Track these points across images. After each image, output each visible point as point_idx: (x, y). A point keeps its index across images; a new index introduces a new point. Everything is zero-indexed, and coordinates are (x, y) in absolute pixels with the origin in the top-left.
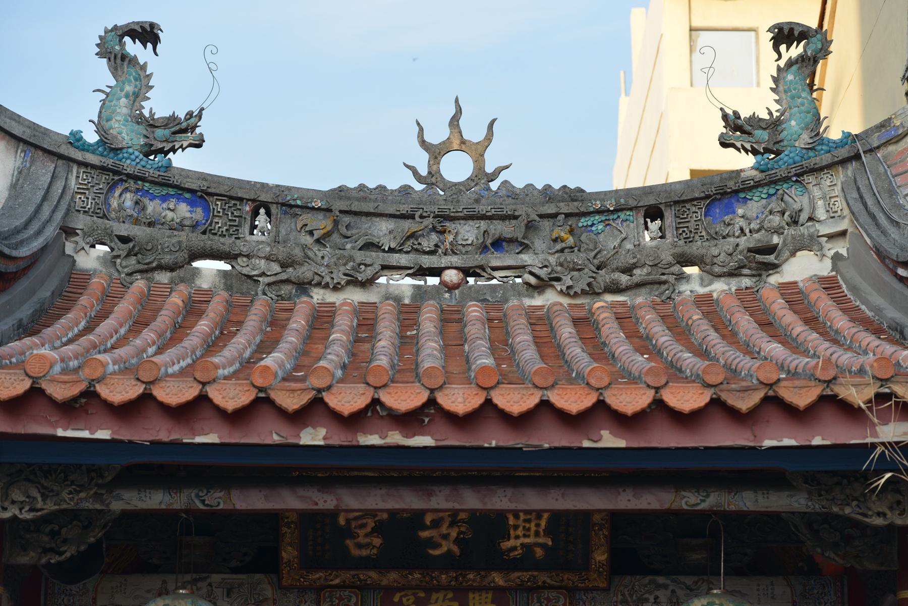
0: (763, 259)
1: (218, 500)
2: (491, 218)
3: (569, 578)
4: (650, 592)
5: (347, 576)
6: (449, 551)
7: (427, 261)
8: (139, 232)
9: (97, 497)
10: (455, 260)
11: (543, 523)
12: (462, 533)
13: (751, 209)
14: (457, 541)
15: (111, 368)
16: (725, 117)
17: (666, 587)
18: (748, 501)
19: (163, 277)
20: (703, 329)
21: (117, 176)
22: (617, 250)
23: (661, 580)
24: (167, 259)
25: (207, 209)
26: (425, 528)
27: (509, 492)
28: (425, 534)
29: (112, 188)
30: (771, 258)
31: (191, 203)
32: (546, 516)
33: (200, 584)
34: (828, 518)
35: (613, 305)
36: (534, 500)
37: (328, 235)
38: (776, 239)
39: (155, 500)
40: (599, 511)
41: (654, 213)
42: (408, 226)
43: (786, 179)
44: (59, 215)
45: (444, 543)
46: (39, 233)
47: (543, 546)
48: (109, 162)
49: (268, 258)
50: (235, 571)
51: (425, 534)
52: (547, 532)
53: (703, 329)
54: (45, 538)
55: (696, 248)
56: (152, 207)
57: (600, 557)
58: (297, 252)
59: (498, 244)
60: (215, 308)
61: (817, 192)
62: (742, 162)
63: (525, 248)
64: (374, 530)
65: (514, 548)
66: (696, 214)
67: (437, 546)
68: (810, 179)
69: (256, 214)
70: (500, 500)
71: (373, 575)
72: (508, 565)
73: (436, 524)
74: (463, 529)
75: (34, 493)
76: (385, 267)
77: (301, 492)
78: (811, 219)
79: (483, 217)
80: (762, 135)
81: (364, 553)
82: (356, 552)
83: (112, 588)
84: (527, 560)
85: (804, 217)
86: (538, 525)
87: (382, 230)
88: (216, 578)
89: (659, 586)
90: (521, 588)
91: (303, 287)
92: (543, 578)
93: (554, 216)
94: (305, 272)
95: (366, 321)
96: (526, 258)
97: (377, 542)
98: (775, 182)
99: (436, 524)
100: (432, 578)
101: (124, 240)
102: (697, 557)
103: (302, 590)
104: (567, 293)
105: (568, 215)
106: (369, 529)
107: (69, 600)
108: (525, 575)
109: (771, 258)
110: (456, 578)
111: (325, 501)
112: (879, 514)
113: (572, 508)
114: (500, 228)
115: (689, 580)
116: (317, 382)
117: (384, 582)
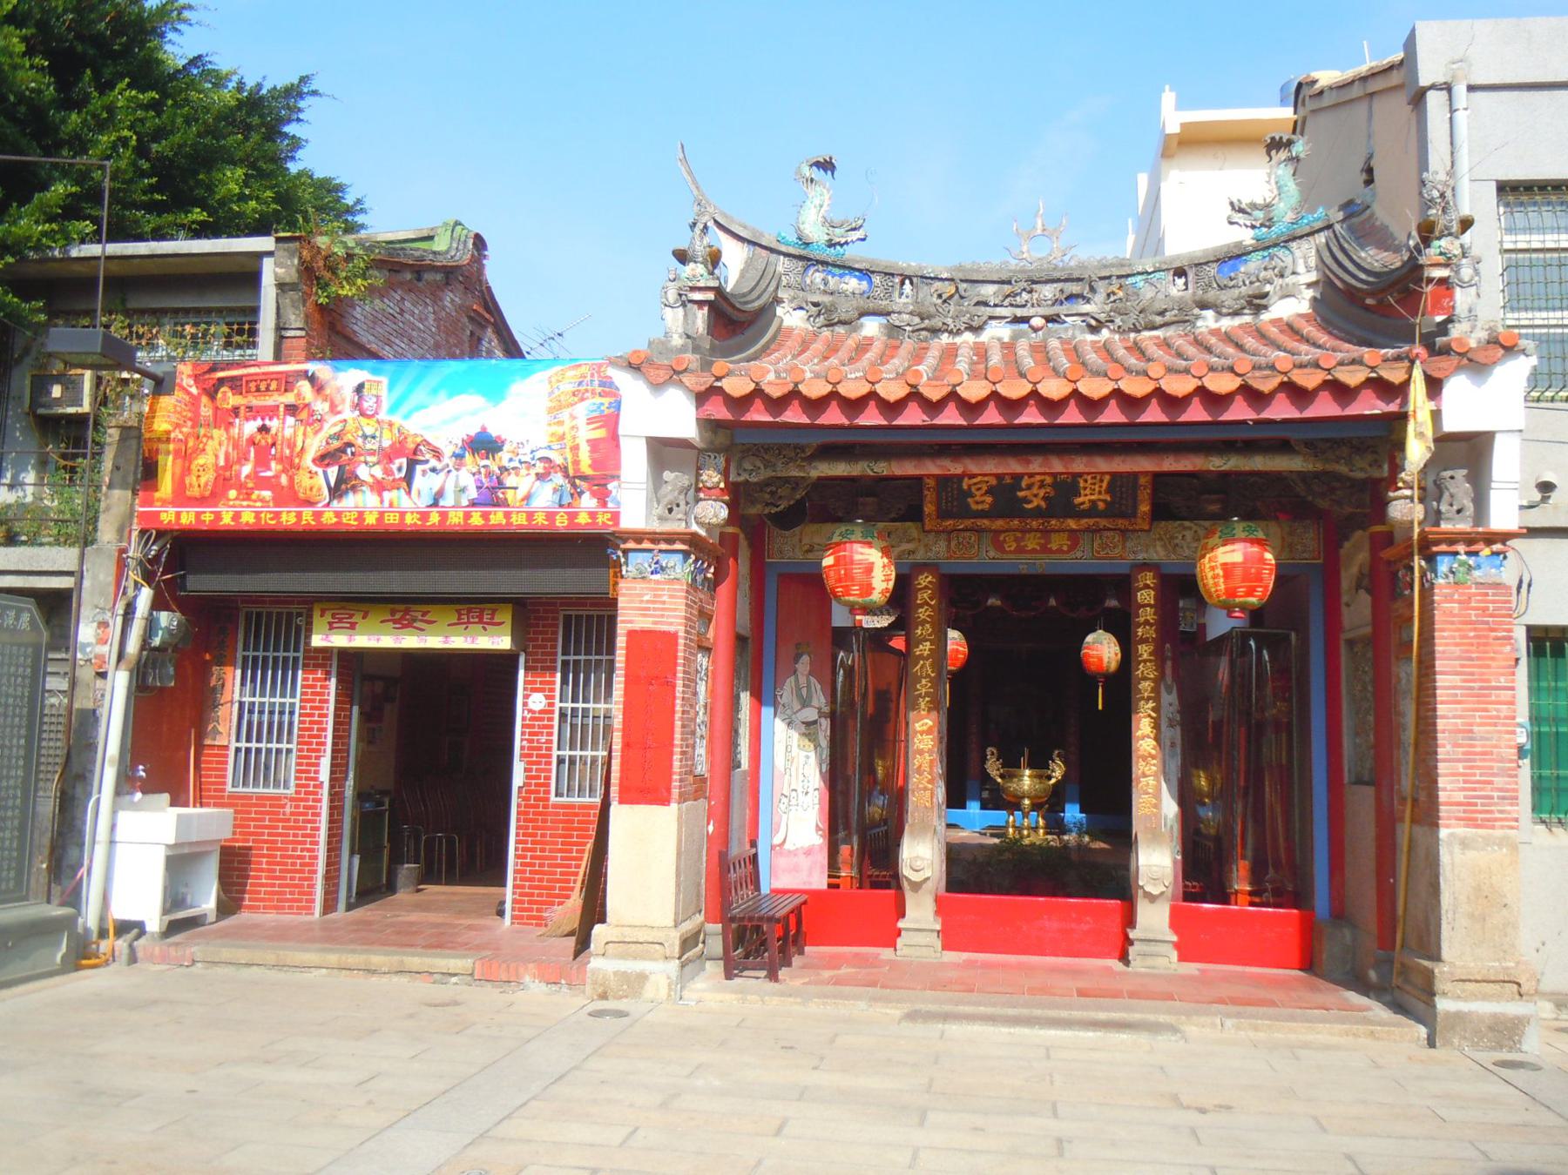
0: (1257, 303)
1: (882, 468)
2: (1066, 280)
3: (1121, 523)
5: (968, 523)
7: (1019, 312)
8: (826, 299)
9: (801, 468)
10: (1042, 311)
11: (1104, 485)
13: (1254, 264)
14: (1044, 498)
15: (808, 375)
16: (1232, 204)
18: (1259, 463)
19: (840, 330)
20: (1219, 346)
21: (808, 261)
22: (1153, 299)
23: (1187, 523)
24: (844, 317)
25: (870, 282)
27: (1085, 459)
28: (1021, 494)
29: (806, 269)
30: (1263, 302)
31: (860, 279)
34: (1325, 473)
35: (1151, 338)
36: (1103, 465)
37: (951, 297)
38: (1268, 288)
39: (840, 469)
40: (1146, 473)
41: (1180, 272)
42: (1007, 289)
43: (1275, 245)
44: (771, 289)
46: (759, 297)
48: (803, 253)
49: (911, 313)
50: (893, 520)
51: (1021, 494)
52: (1108, 491)
53: (1219, 346)
54: (767, 496)
55: (1212, 295)
56: (832, 281)
57: (1145, 508)
58: (932, 310)
59: (1071, 297)
60: (877, 348)
61: (1298, 253)
62: (1246, 237)
63: (1088, 301)
66: (1212, 270)
67: (1030, 502)
68: (1294, 245)
69: (902, 283)
70: (1079, 465)
72: (1080, 514)
73: (1029, 487)
75: (759, 464)
76: (991, 318)
77: (939, 462)
78: (1294, 273)
79: (1058, 280)
80: (1260, 214)
81: (980, 507)
82: (974, 507)
84: (1093, 511)
85: (1288, 272)
87: (989, 291)
88: (881, 525)
89: (1185, 528)
90: (1088, 530)
91: (935, 332)
92: (1103, 522)
93: (1109, 277)
94: (937, 322)
95: (982, 352)
96: (1086, 308)
97: (989, 499)
98: (1268, 248)
99: (1029, 487)
101: (815, 305)
102: (1214, 508)
103: (938, 532)
104: (1119, 330)
105: (1119, 277)
108: (1091, 521)
109: (1263, 302)
111: (955, 468)
112: (1362, 469)
114: (1074, 288)
115: (1207, 524)
116: (955, 380)
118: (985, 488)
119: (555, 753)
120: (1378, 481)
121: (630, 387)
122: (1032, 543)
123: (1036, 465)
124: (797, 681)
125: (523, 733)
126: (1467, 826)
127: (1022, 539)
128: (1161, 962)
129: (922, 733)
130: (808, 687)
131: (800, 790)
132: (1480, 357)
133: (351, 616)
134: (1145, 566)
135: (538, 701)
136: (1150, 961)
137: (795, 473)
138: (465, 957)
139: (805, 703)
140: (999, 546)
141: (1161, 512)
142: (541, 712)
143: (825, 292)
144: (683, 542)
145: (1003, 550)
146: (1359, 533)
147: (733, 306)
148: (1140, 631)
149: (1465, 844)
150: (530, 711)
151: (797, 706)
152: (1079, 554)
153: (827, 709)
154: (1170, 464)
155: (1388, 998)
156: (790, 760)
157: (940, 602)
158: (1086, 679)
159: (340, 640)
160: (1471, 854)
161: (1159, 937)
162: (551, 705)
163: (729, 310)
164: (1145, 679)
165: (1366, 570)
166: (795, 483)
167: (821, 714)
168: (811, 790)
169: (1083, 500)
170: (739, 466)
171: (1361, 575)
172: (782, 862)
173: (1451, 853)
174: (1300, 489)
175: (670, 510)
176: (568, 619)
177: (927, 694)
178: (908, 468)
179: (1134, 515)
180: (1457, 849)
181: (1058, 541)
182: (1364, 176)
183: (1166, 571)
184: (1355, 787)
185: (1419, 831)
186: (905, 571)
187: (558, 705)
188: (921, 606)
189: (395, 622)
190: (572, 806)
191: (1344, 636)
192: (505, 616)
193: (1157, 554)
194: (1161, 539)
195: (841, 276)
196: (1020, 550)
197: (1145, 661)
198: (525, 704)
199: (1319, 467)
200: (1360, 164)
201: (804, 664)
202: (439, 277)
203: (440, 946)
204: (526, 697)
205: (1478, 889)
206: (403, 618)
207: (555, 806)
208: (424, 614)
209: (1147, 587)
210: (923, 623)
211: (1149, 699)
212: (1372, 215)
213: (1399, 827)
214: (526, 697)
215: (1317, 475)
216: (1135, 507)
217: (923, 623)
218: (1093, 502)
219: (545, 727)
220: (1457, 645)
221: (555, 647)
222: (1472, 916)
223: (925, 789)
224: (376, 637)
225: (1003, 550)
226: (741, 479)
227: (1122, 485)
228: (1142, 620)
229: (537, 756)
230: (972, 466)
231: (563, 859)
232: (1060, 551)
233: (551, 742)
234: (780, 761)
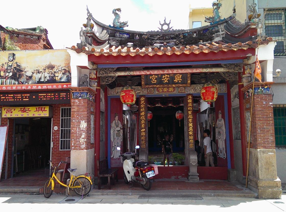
3: (184, 85)
4: (196, 87)
11: (180, 77)
14: (168, 80)
17: (199, 86)
18: (214, 70)
23: (198, 85)
27: (176, 70)
28: (163, 79)
30: (212, 38)
34: (228, 72)
36: (180, 71)
39: (122, 74)
50: (135, 86)
51: (163, 79)
56: (121, 35)
57: (189, 82)
70: (175, 71)
72: (175, 83)
73: (164, 78)
75: (104, 72)
77: (144, 72)
82: (153, 82)
84: (178, 83)
92: (180, 85)
97: (156, 81)
99: (164, 78)
101: (117, 40)
102: (204, 81)
103: (145, 88)
106: (154, 79)
111: (148, 73)
119: (60, 140)
120: (239, 73)
121: (73, 54)
122: (165, 90)
123: (166, 72)
124: (115, 121)
125: (53, 135)
126: (264, 148)
127: (163, 89)
128: (195, 180)
129: (143, 132)
130: (118, 123)
133: (11, 110)
134: (189, 94)
135: (56, 128)
136: (193, 180)
137: (113, 75)
138: (37, 188)
139: (117, 126)
140: (158, 91)
141: (193, 83)
142: (57, 130)
143: (119, 38)
144: (86, 90)
145: (159, 92)
146: (235, 86)
147: (98, 38)
148: (189, 108)
149: (264, 152)
150: (54, 130)
151: (115, 127)
152: (175, 92)
153: (122, 128)
154: (195, 71)
156: (114, 139)
158: (177, 120)
159: (9, 115)
160: (265, 155)
161: (195, 174)
162: (59, 129)
163: (97, 39)
164: (190, 118)
165: (237, 93)
166: (113, 77)
167: (121, 129)
168: (119, 145)
169: (176, 80)
170: (99, 73)
171: (236, 95)
172: (113, 161)
173: (260, 154)
174: (223, 75)
175: (83, 83)
176: (62, 109)
177: (144, 123)
178: (137, 73)
179: (187, 83)
180: (262, 153)
181: (171, 89)
182: (233, 11)
184: (237, 140)
185: (252, 150)
186: (138, 97)
187: (61, 129)
188: (142, 104)
189: (21, 111)
190: (65, 151)
191: (232, 108)
192: (47, 108)
193: (192, 92)
195: (123, 34)
197: (190, 115)
198: (53, 129)
199: (227, 70)
200: (232, 9)
201: (117, 118)
202: (37, 37)
203: (33, 186)
204: (53, 127)
205: (267, 162)
206: (23, 110)
207: (60, 151)
208: (28, 109)
209: (190, 99)
211: (191, 123)
212: (235, 19)
213: (247, 149)
214: (53, 127)
215: (226, 72)
216: (187, 82)
219: (58, 134)
220: (260, 108)
221: (60, 116)
222: (266, 169)
223: (144, 144)
224: (17, 113)
225: (159, 92)
226: (100, 76)
227: (184, 76)
228: (189, 106)
229: (56, 141)
230: (152, 72)
231: (262, 129)
233: (59, 137)
234: (112, 140)
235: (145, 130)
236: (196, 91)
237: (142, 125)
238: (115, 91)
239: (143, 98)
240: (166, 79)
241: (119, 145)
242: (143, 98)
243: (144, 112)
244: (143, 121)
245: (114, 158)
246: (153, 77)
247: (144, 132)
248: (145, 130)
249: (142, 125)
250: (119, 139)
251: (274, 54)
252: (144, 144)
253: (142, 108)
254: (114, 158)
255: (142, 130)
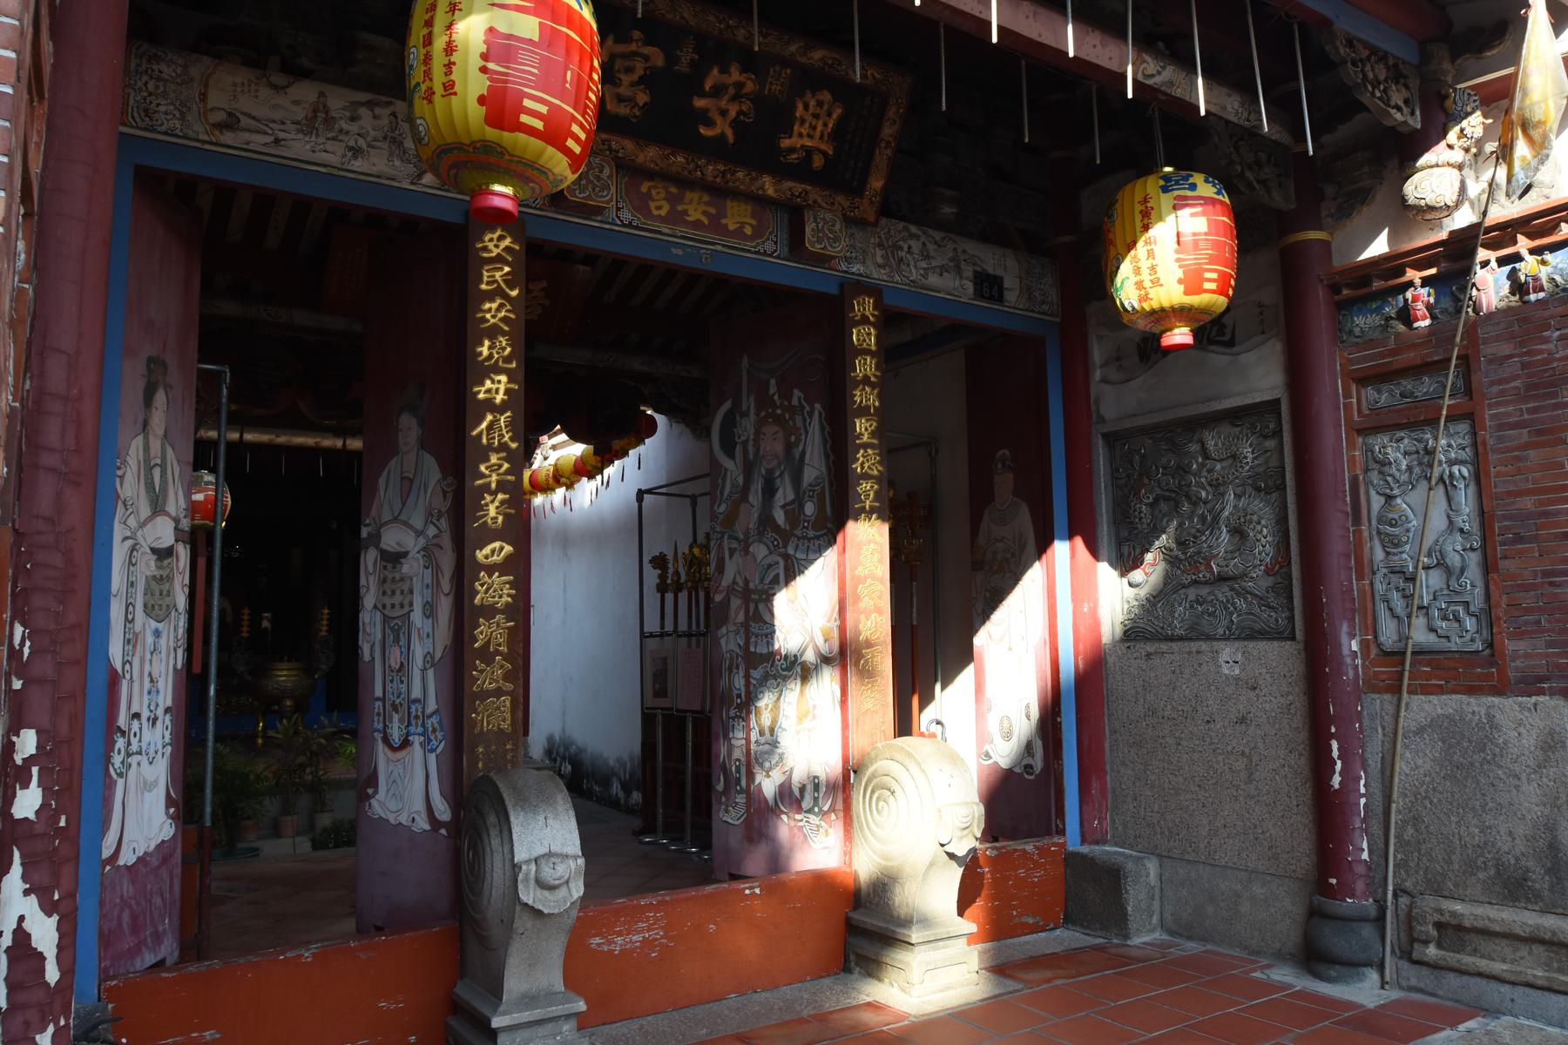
4: (905, 241)
6: (723, 134)
12: (744, 114)
14: (735, 124)
17: (917, 237)
26: (703, 95)
28: (699, 103)
32: (203, 433)
33: (378, 111)
45: (719, 121)
47: (824, 153)
51: (699, 103)
64: (641, 80)
65: (792, 150)
67: (710, 123)
71: (629, 145)
72: (782, 171)
74: (744, 108)
83: (235, 85)
84: (801, 171)
86: (825, 125)
99: (717, 91)
100: (697, 166)
106: (635, 77)
107: (157, 87)
110: (724, 173)
113: (1034, 36)
117: (640, 159)
118: (639, 72)
124: (147, 448)
127: (680, 199)
129: (490, 569)
131: (145, 714)
132: (164, 573)
139: (158, 508)
145: (646, 212)
152: (769, 247)
155: (155, 862)
156: (131, 641)
157: (527, 291)
164: (866, 476)
183: (889, 300)
188: (490, 296)
194: (881, 245)
196: (675, 218)
197: (865, 446)
209: (864, 320)
210: (493, 332)
217: (493, 332)
218: (809, 152)
223: (498, 693)
225: (646, 212)
232: (739, 234)
235: (508, 549)
236: (899, 271)
237: (488, 498)
238: (203, 97)
239: (499, 233)
240: (723, 103)
241: (160, 712)
242: (501, 238)
243: (504, 378)
244: (494, 459)
245: (121, 862)
246: (623, 56)
247: (503, 568)
248: (508, 549)
249: (488, 498)
250: (164, 635)
251: (1516, 74)
252: (498, 693)
253: (492, 338)
254: (121, 862)
255: (487, 550)
